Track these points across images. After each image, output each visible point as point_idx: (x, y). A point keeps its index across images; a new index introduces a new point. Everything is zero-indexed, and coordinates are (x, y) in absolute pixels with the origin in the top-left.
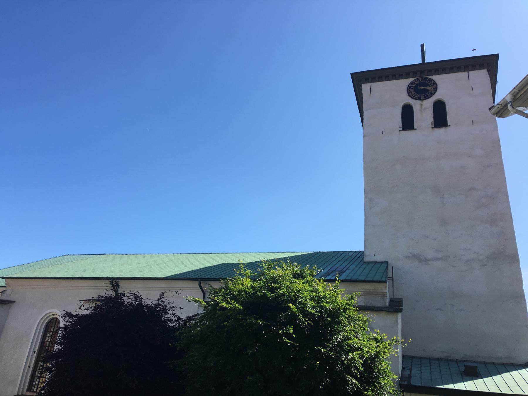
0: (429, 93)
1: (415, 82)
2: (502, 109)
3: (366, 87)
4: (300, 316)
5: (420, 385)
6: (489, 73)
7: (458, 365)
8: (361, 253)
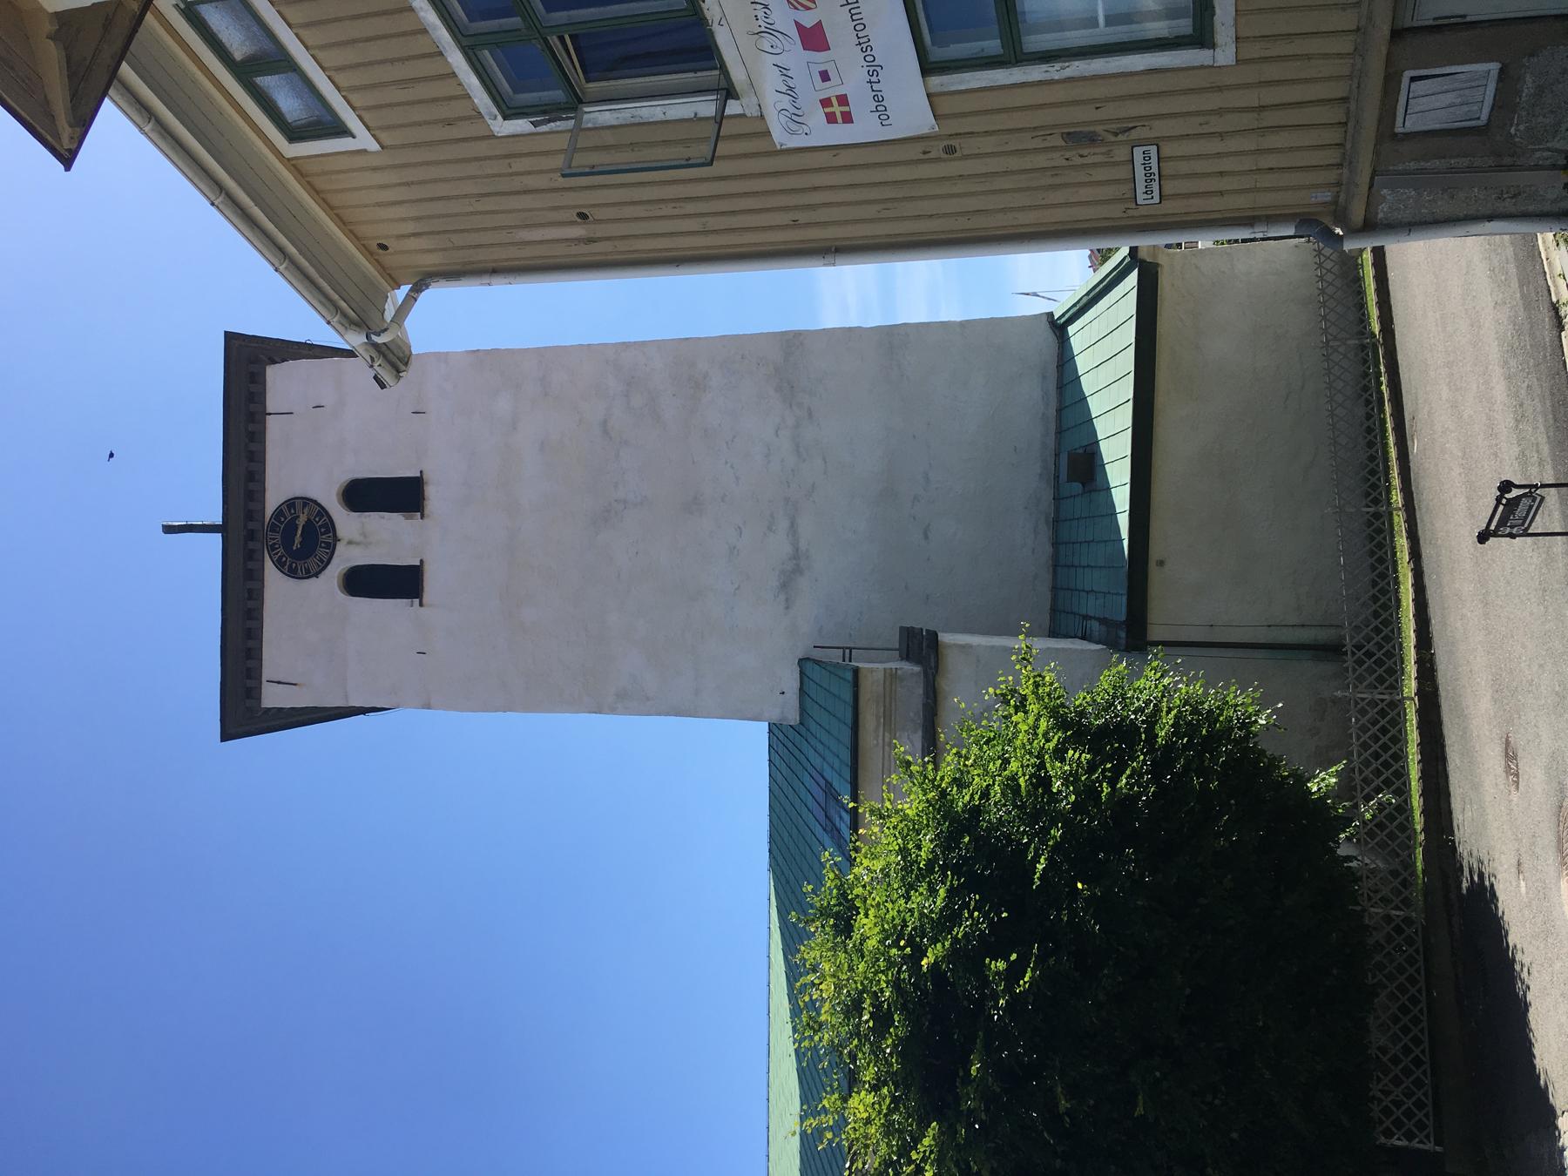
0: (317, 519)
1: (277, 556)
2: (385, 356)
3: (273, 697)
4: (958, 933)
5: (1124, 599)
6: (277, 359)
7: (1067, 498)
8: (776, 731)
